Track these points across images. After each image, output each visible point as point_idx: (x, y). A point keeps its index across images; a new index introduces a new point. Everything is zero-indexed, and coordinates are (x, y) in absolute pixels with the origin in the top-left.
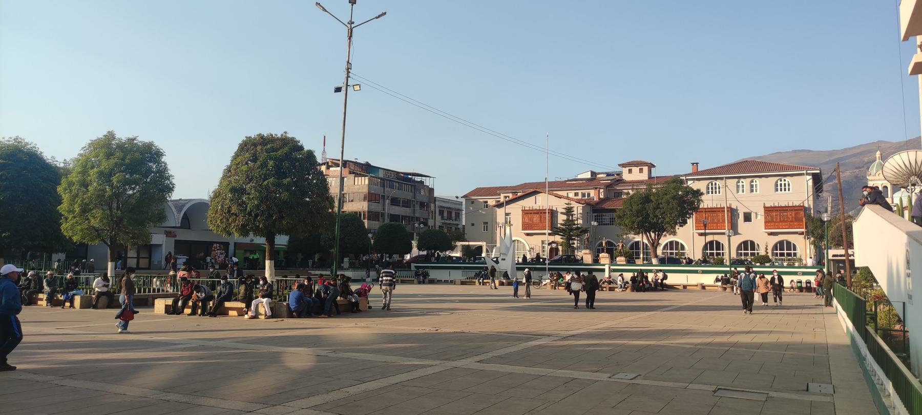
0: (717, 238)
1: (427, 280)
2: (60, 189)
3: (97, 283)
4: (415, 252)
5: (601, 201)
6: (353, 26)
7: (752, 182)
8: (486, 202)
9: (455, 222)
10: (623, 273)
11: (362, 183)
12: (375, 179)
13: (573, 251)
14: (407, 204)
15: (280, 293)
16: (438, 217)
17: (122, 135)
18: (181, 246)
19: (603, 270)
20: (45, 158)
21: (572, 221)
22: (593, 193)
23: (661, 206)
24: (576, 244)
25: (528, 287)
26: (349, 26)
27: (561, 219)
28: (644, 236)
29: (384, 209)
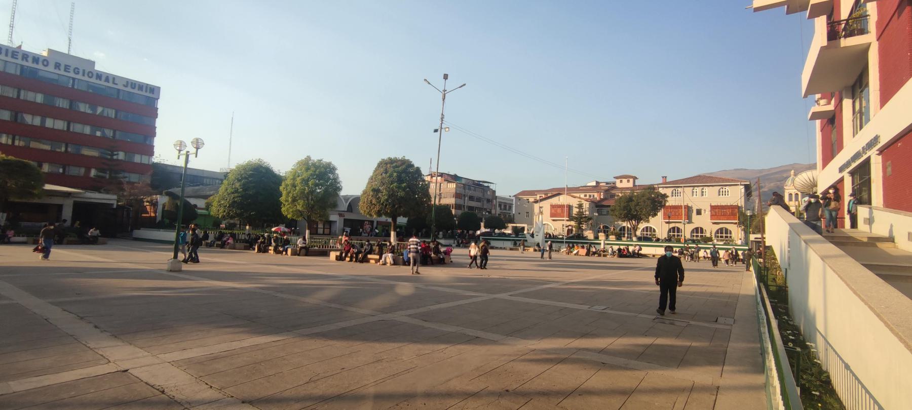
0: (677, 225)
2: (281, 188)
3: (300, 242)
4: (483, 230)
5: (602, 200)
6: (446, 92)
7: (694, 189)
8: (528, 200)
9: (508, 212)
10: (613, 246)
11: (452, 186)
13: (582, 232)
14: (479, 200)
15: (399, 251)
16: (498, 209)
17: (315, 158)
18: (347, 222)
19: (600, 244)
20: (274, 171)
21: (582, 212)
22: (596, 195)
23: (640, 204)
24: (584, 227)
25: (550, 252)
26: (443, 92)
27: (575, 211)
28: (628, 223)
29: (465, 203)
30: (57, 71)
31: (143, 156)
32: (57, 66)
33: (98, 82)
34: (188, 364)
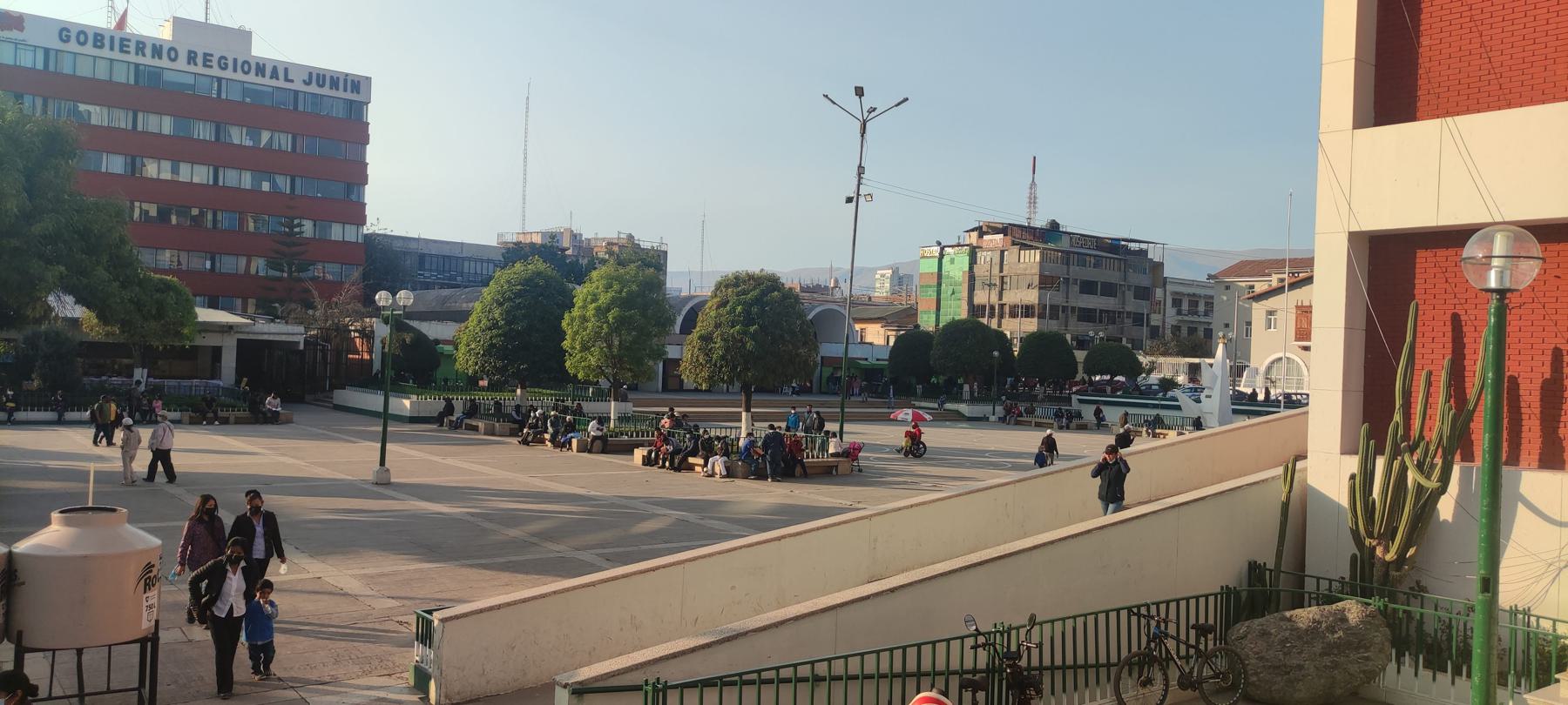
1: (1073, 425)
2: (564, 324)
9: (1203, 319)
11: (1032, 258)
12: (1052, 252)
14: (1109, 290)
16: (1171, 311)
30: (192, 68)
31: (347, 227)
32: (192, 57)
33: (259, 80)
34: (369, 579)
